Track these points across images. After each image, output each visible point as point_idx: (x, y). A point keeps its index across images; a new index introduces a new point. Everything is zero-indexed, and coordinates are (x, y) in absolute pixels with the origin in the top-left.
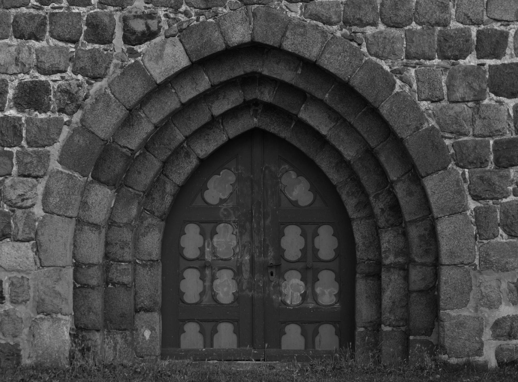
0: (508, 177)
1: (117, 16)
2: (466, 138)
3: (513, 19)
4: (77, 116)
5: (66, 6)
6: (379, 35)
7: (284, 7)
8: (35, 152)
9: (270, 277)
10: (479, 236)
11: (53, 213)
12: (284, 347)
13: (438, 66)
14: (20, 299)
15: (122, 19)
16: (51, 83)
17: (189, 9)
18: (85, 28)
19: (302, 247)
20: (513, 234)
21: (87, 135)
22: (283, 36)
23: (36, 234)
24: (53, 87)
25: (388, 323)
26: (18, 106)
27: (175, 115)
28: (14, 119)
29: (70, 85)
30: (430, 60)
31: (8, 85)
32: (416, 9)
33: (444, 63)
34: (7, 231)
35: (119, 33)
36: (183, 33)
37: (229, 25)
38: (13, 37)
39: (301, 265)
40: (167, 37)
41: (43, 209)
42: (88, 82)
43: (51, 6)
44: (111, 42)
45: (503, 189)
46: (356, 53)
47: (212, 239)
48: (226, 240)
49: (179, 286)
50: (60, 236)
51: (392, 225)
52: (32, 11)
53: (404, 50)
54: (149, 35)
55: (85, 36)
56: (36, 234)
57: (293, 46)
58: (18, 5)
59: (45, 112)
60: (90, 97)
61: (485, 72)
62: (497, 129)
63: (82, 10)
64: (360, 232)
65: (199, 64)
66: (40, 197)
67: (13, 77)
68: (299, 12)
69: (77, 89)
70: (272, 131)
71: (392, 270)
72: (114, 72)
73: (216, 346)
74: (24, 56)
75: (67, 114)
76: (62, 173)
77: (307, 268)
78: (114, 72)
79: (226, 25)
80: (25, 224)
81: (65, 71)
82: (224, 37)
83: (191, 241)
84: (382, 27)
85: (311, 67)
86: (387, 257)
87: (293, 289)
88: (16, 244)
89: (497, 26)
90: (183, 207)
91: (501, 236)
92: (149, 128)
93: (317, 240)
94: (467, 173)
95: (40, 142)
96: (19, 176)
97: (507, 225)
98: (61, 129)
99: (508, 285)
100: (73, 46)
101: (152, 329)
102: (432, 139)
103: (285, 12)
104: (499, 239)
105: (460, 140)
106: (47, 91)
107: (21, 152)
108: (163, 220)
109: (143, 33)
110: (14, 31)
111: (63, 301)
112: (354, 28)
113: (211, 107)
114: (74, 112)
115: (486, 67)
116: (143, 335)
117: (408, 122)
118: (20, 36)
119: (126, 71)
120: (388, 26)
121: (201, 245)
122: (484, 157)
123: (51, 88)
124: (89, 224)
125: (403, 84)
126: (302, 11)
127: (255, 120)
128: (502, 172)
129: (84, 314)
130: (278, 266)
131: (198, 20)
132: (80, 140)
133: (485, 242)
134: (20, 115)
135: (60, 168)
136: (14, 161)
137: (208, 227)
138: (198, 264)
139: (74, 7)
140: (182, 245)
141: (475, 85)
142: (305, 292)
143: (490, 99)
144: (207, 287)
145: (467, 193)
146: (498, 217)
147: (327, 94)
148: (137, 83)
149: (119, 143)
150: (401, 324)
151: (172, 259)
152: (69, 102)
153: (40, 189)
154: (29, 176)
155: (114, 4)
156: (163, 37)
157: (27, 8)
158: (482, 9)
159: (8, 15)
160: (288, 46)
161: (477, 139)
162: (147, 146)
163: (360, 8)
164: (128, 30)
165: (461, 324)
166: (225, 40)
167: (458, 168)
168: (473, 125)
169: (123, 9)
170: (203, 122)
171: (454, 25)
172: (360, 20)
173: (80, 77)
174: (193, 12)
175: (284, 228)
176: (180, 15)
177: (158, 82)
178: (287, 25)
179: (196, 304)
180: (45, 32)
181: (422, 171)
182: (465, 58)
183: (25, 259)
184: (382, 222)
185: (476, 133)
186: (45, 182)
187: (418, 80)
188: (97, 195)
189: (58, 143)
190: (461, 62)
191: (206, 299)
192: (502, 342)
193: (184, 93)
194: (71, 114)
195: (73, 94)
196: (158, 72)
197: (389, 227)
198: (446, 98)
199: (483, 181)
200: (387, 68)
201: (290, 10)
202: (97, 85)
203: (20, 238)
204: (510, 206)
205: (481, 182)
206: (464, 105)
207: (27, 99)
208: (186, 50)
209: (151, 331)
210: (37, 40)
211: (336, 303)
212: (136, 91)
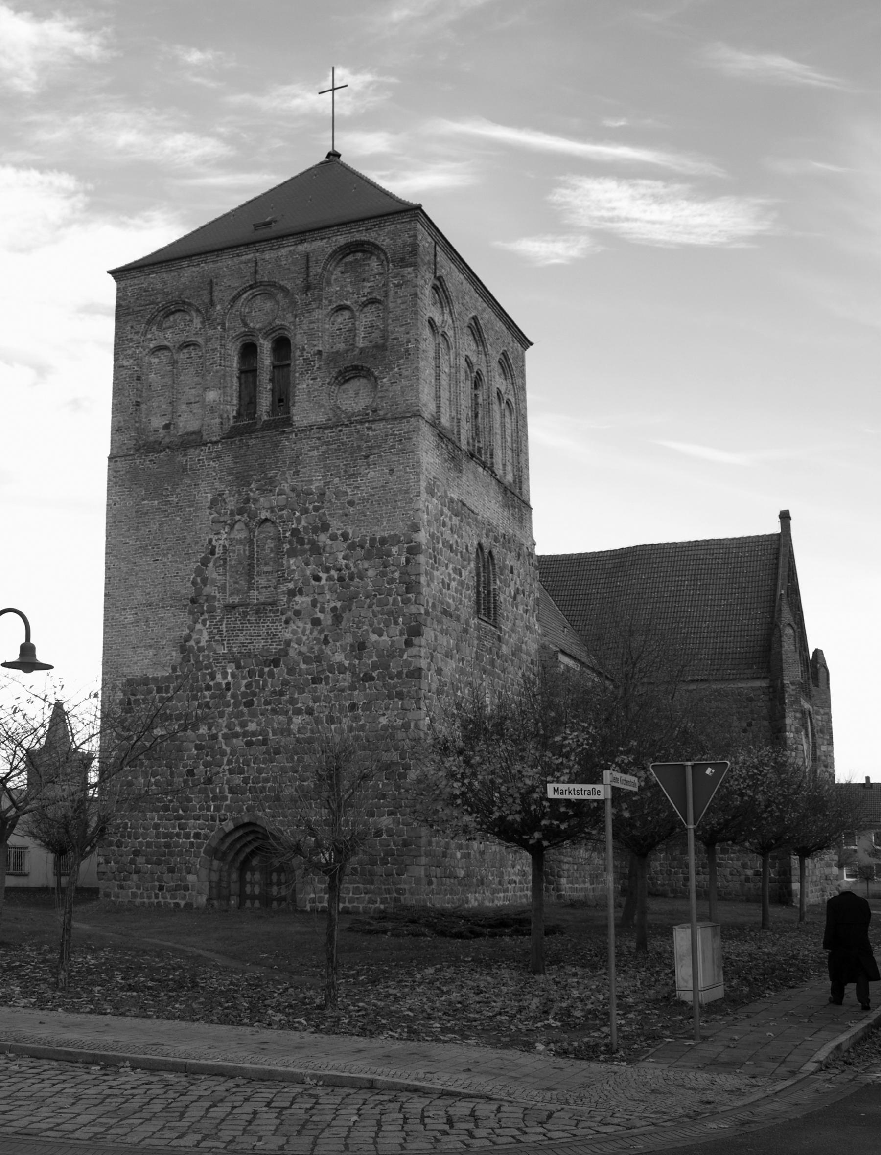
36: (233, 819)
48: (257, 876)
50: (204, 873)
54: (225, 820)
65: (237, 828)
72: (216, 829)
78: (216, 829)
83: (248, 876)
90: (244, 867)
196: (227, 830)
212: (222, 835)
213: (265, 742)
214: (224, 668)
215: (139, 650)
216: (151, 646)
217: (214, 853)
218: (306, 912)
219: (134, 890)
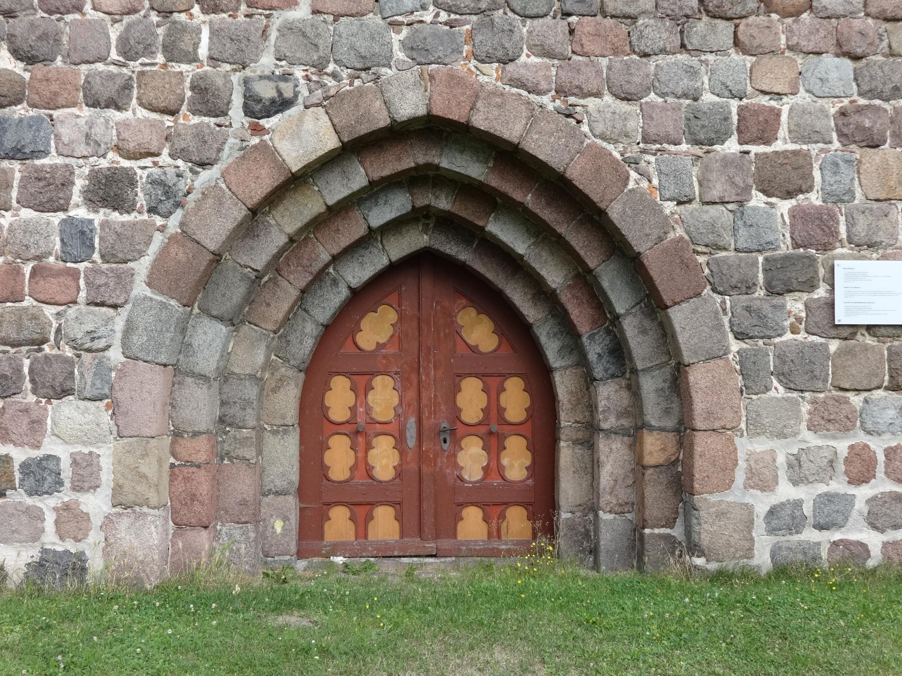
0: (783, 307)
1: (236, 78)
2: (724, 254)
3: (786, 91)
5: (162, 62)
6: (606, 110)
7: (473, 69)
8: (112, 270)
9: (443, 444)
10: (746, 390)
11: (137, 359)
12: (460, 537)
13: (686, 154)
14: (86, 485)
15: (242, 81)
16: (139, 172)
17: (338, 69)
18: (189, 94)
19: (483, 407)
20: (792, 386)
21: (190, 244)
22: (472, 109)
23: (112, 388)
24: (141, 177)
25: (608, 509)
26: (89, 203)
27: (317, 224)
28: (82, 222)
29: (165, 173)
30: (675, 145)
31: (74, 173)
32: (656, 75)
33: (697, 150)
34: (68, 385)
35: (237, 101)
36: (329, 103)
37: (395, 91)
38: (84, 105)
39: (483, 430)
40: (306, 107)
41: (123, 353)
42: (191, 170)
43: (140, 61)
44: (227, 114)
45: (777, 324)
46: (575, 133)
47: (366, 396)
48: (384, 397)
49: (322, 458)
51: (613, 376)
52: (113, 68)
53: (640, 130)
54: (282, 104)
55: (189, 104)
56: (112, 388)
57: (486, 122)
58: (91, 60)
59: (128, 213)
60: (194, 191)
61: (751, 162)
62: (768, 240)
63: (184, 67)
64: (565, 384)
66: (119, 335)
67: (81, 161)
68: (495, 75)
69: (176, 179)
70: (448, 251)
71: (613, 436)
72: (229, 155)
73: (371, 537)
74: (98, 131)
75: (162, 216)
76: (151, 299)
77: (491, 433)
78: (229, 155)
79: (392, 92)
80: (95, 374)
81: (158, 155)
82: (388, 109)
83: (339, 398)
84: (608, 98)
85: (508, 155)
86: (606, 420)
87: (472, 459)
88: (82, 404)
89: (764, 100)
91: (776, 388)
92: (282, 240)
93: (503, 397)
94: (728, 302)
95: (120, 255)
96: (88, 304)
97: (783, 374)
98: (151, 237)
99: (787, 457)
100: (171, 118)
101: (285, 519)
102: (680, 255)
103: (474, 76)
104: (772, 393)
105: (717, 256)
106: (132, 183)
107: (92, 270)
108: (301, 371)
109: (273, 101)
110: (85, 96)
111: (150, 487)
112: (572, 100)
113: (368, 215)
114: (171, 213)
115: (752, 155)
116: (273, 528)
117: (648, 231)
119: (246, 154)
120: (617, 97)
121: (352, 404)
122: (752, 279)
123: (138, 178)
124: (193, 374)
125: (639, 177)
126: (498, 74)
127: (425, 236)
128: (777, 300)
129: (186, 504)
130: (453, 431)
131: (351, 84)
132: (179, 253)
133: (754, 397)
134: (91, 216)
135: (148, 292)
136: (82, 282)
137: (361, 380)
138: (347, 429)
139: (174, 64)
140: (327, 404)
141: (738, 180)
142: (488, 465)
143: (757, 200)
144: (359, 459)
145: (729, 330)
146: (772, 363)
147: (530, 195)
148: (263, 172)
149: (239, 261)
150: (626, 510)
151: (313, 424)
152: (163, 198)
153: (119, 324)
154: (102, 304)
155: (231, 60)
156: (302, 107)
157: (106, 64)
158: (744, 76)
159: (77, 74)
160: (480, 121)
161: (740, 254)
162: (276, 265)
163: (579, 71)
164: (251, 96)
165: (721, 514)
166: (389, 112)
167: (715, 295)
168: (735, 235)
169: (244, 68)
170: (357, 236)
171: (708, 98)
172: (579, 87)
173: (180, 162)
174: (345, 73)
175: (461, 381)
176: (326, 77)
177: (293, 171)
178: (476, 94)
179: (346, 481)
180: (131, 99)
181: (666, 298)
182: (723, 142)
183: (95, 426)
184: (598, 372)
185: (740, 245)
186: (126, 313)
187: (660, 172)
188: (205, 333)
189: (146, 257)
190: (717, 147)
191: (361, 479)
192: (777, 539)
193: (330, 191)
194: (166, 215)
195: (170, 187)
197: (608, 379)
198: (698, 200)
199: (750, 312)
200: (617, 156)
201: (481, 72)
202: (205, 175)
203: (88, 396)
204: (788, 347)
205: (747, 314)
206: (721, 208)
207: (101, 192)
208: (334, 125)
209: (284, 522)
210: (119, 108)
211: (528, 478)
217: (198, 280)
218: (748, 575)
219: (838, 486)
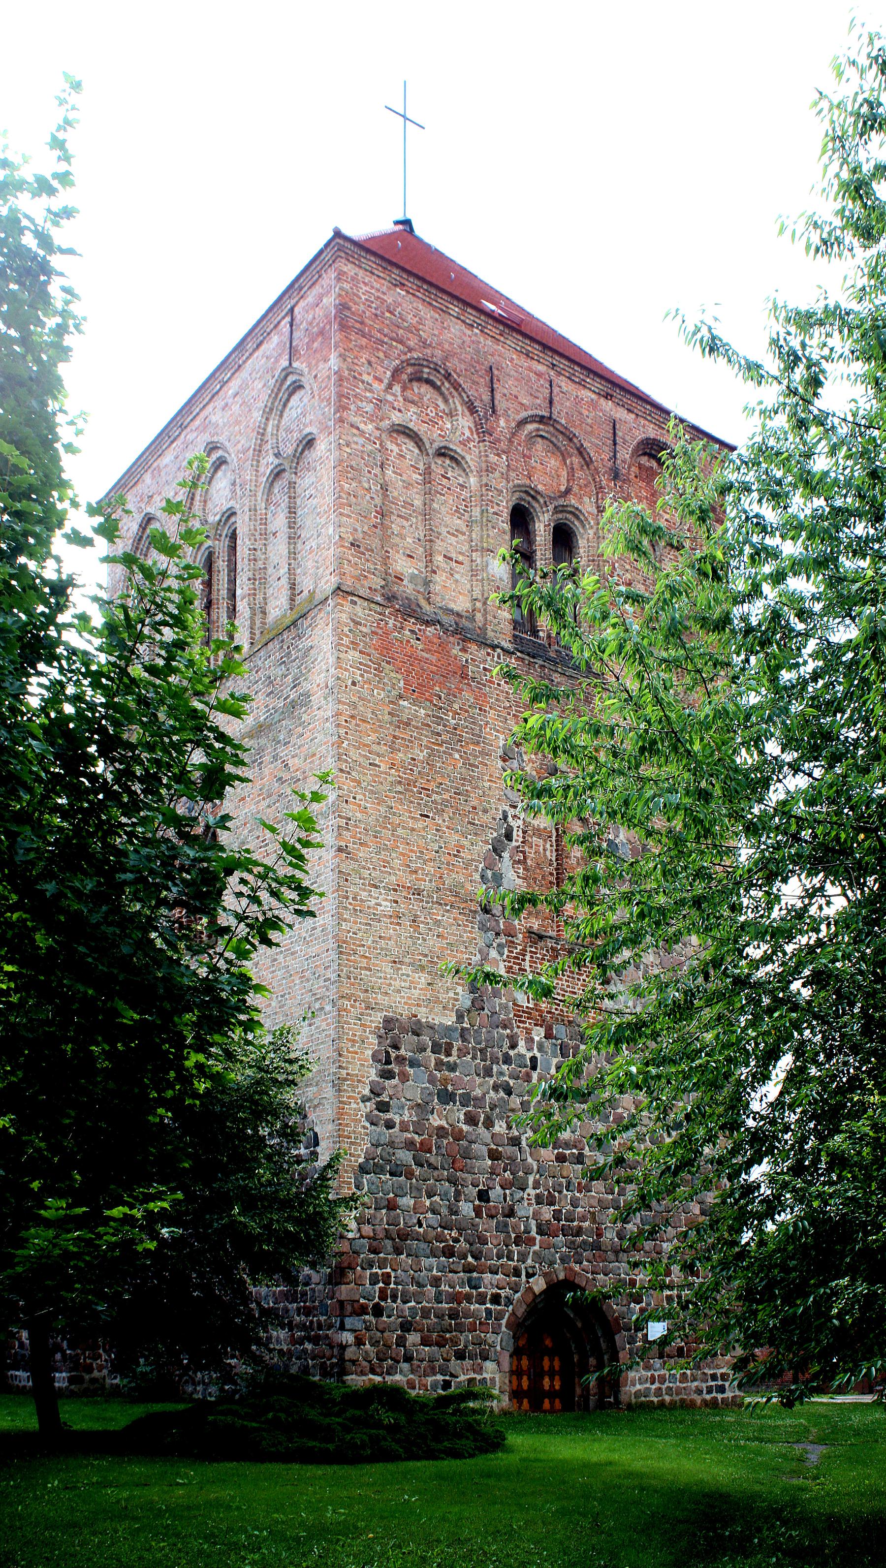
4: (511, 1308)
35: (524, 1273)
36: (545, 1275)
54: (534, 1275)
72: (522, 1290)
78: (522, 1290)
118: (491, 1273)
213: (580, 1159)
214: (528, 1031)
215: (405, 969)
216: (422, 968)
